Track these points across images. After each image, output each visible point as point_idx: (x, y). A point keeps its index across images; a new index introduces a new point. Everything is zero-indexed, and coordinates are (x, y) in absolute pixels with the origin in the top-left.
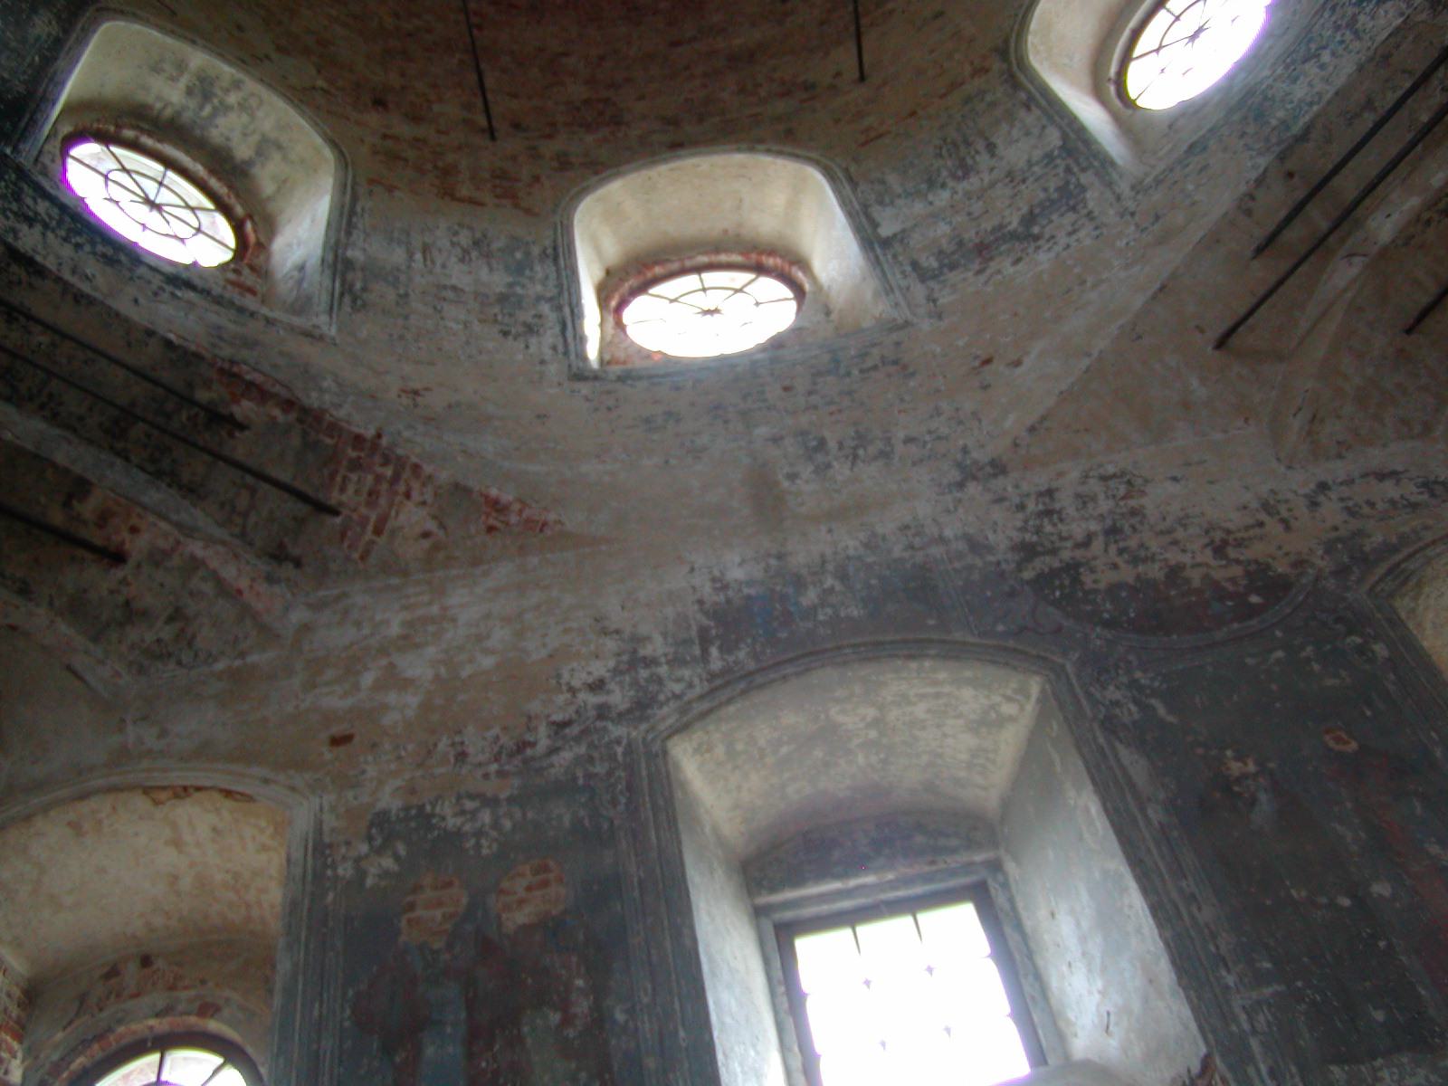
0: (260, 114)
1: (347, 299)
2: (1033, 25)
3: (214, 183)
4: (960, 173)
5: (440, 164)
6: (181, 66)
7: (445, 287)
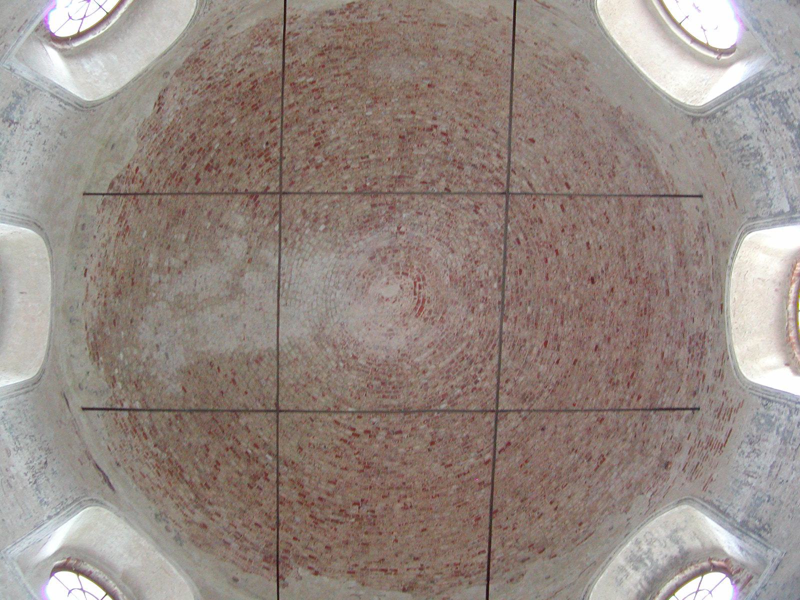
0: (656, 535)
1: (763, 534)
2: (682, 100)
3: (688, 572)
4: (759, 158)
5: (705, 445)
6: (622, 569)
7: (770, 472)
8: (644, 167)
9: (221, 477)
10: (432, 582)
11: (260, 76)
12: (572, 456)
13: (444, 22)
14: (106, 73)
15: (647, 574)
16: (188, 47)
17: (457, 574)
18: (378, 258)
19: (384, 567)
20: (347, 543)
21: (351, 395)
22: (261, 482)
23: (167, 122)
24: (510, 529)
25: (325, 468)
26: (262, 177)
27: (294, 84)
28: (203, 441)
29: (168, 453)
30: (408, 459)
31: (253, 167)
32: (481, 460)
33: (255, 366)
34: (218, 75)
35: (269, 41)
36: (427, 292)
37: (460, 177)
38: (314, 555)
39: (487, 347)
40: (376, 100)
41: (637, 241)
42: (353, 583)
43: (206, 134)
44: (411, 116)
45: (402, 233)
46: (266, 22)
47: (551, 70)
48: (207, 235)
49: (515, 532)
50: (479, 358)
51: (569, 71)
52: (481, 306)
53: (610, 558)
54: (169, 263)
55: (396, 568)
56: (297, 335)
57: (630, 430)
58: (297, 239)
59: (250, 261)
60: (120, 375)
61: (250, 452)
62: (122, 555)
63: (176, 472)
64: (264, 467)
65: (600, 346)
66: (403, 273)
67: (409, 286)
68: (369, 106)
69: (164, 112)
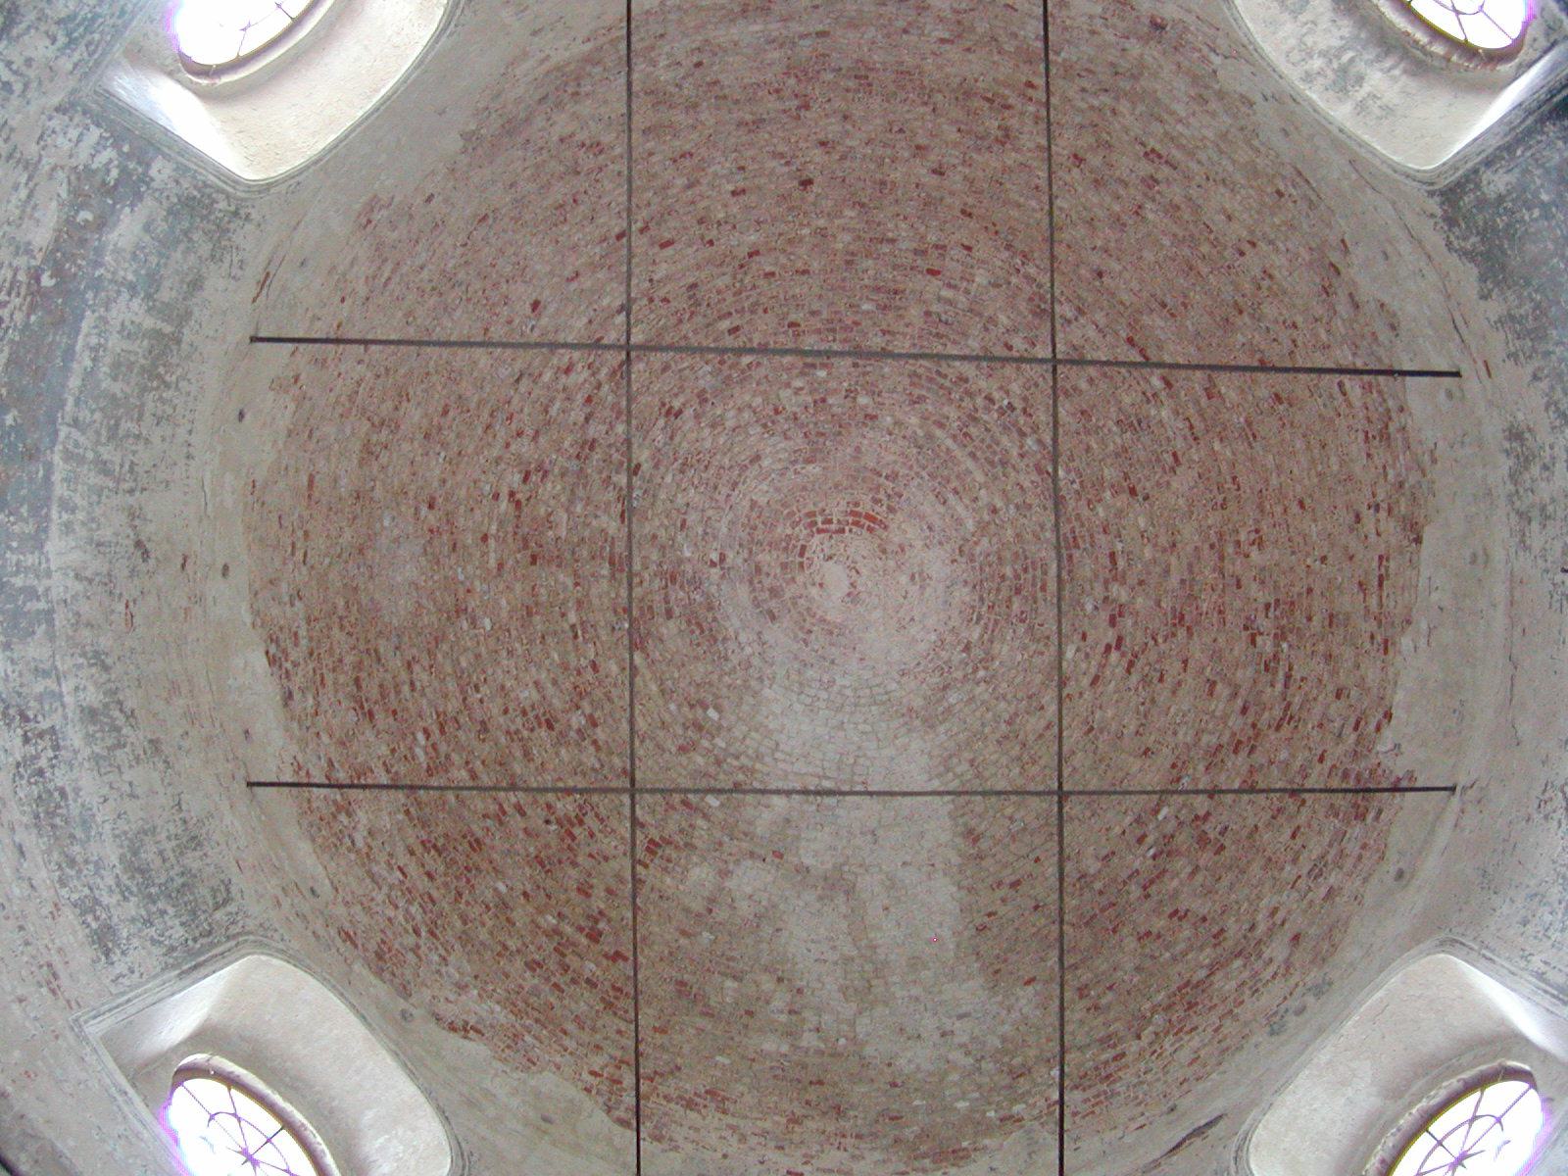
6: (1361, 107)
8: (579, 85)
9: (1200, 906)
10: (1401, 485)
11: (412, 836)
12: (1151, 216)
13: (305, 480)
14: (400, 1132)
15: (1371, 57)
16: (351, 971)
17: (1385, 436)
18: (773, 604)
19: (1376, 583)
20: (1329, 657)
21: (1042, 654)
22: (1211, 829)
23: (502, 1016)
24: (1295, 333)
25: (1185, 702)
26: (613, 831)
27: (429, 769)
28: (1131, 943)
29: (1154, 1010)
30: (1163, 541)
31: (594, 850)
32: (1163, 395)
33: (984, 844)
34: (408, 914)
35: (343, 817)
36: (837, 509)
37: (610, 446)
38: (1352, 720)
39: (942, 387)
40: (460, 611)
41: (725, 97)
42: (1405, 642)
43: (528, 940)
44: (492, 542)
45: (723, 558)
46: (305, 824)
47: (393, 271)
48: (727, 938)
49: (1300, 324)
50: (964, 404)
51: (395, 235)
52: (863, 400)
53: (1341, 131)
54: (782, 1012)
55: (1376, 558)
56: (924, 760)
57: (1096, 103)
58: (736, 763)
59: (779, 855)
60: (999, 1107)
61: (1152, 852)
62: (1350, 1101)
63: (1190, 997)
64: (1181, 824)
65: (935, 166)
66: (802, 555)
67: (827, 544)
68: (474, 623)
69: (481, 1020)
